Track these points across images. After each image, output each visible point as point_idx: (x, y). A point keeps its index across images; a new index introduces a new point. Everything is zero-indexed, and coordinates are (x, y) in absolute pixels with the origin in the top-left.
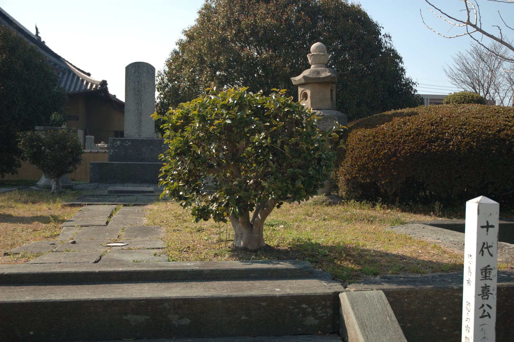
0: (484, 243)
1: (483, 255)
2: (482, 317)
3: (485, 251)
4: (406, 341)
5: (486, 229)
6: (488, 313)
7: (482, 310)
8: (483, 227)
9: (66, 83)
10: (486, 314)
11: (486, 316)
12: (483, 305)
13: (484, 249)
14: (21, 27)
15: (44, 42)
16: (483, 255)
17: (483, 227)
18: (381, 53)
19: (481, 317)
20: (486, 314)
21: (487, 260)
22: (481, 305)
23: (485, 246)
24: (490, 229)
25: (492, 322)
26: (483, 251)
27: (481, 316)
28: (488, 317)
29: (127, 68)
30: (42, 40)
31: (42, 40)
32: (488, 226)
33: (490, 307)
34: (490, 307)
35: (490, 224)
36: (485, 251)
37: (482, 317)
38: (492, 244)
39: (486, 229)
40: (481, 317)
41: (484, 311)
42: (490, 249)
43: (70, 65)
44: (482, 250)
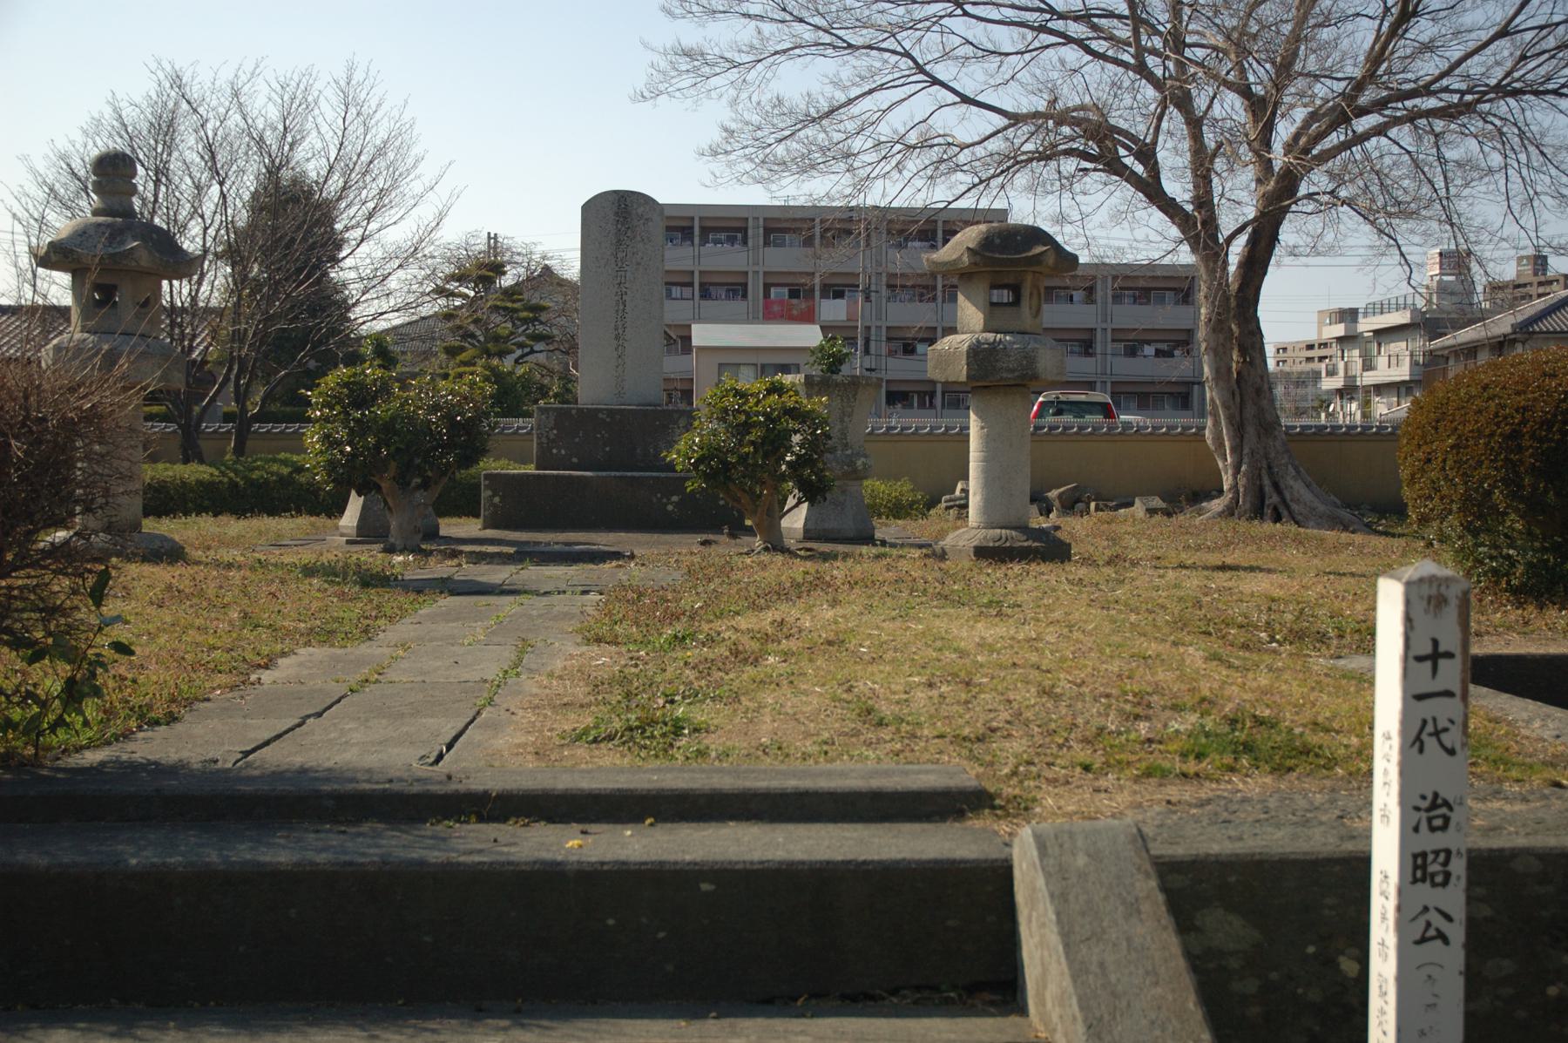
0: (1425, 722)
1: (1421, 751)
2: (1423, 940)
3: (1430, 743)
4: (1206, 1036)
5: (1428, 665)
6: (1438, 930)
7: (1421, 923)
8: (1419, 659)
10: (1432, 932)
11: (1432, 938)
12: (1426, 909)
13: (1424, 737)
16: (1421, 751)
17: (1419, 659)
19: (1417, 943)
20: (1432, 932)
21: (1446, 776)
22: (1420, 909)
23: (1430, 728)
24: (1442, 663)
25: (1453, 957)
26: (1422, 743)
27: (1418, 937)
28: (1439, 943)
29: (587, 208)
32: (1435, 656)
33: (1449, 918)
34: (1449, 918)
35: (1442, 649)
36: (1430, 743)
37: (1423, 940)
38: (1448, 725)
39: (1428, 665)
40: (1417, 943)
41: (1428, 924)
42: (1444, 736)
43: (572, 844)
44: (1418, 738)
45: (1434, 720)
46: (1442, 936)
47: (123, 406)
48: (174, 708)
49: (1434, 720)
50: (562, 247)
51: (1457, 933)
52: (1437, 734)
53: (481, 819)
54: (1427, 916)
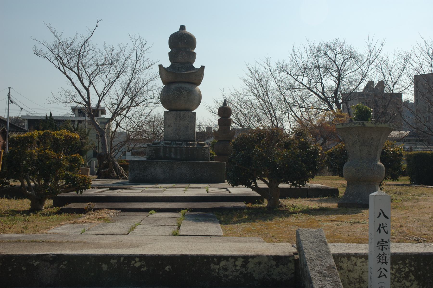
0: (380, 225)
1: (380, 232)
2: (380, 277)
3: (382, 230)
7: (380, 272)
9: (99, 187)
12: (381, 269)
13: (380, 228)
14: (235, 195)
15: (194, 54)
16: (380, 232)
18: (252, 182)
19: (378, 277)
23: (382, 226)
27: (378, 276)
28: (384, 277)
30: (195, 51)
31: (197, 65)
33: (386, 270)
34: (386, 270)
37: (380, 277)
40: (378, 277)
41: (381, 272)
42: (385, 228)
45: (383, 224)
46: (385, 275)
47: (63, 126)
48: (22, 230)
49: (383, 224)
50: (197, 65)
51: (388, 274)
52: (383, 227)
53: (38, 120)
54: (381, 270)
